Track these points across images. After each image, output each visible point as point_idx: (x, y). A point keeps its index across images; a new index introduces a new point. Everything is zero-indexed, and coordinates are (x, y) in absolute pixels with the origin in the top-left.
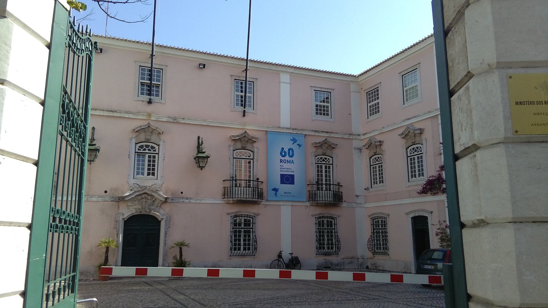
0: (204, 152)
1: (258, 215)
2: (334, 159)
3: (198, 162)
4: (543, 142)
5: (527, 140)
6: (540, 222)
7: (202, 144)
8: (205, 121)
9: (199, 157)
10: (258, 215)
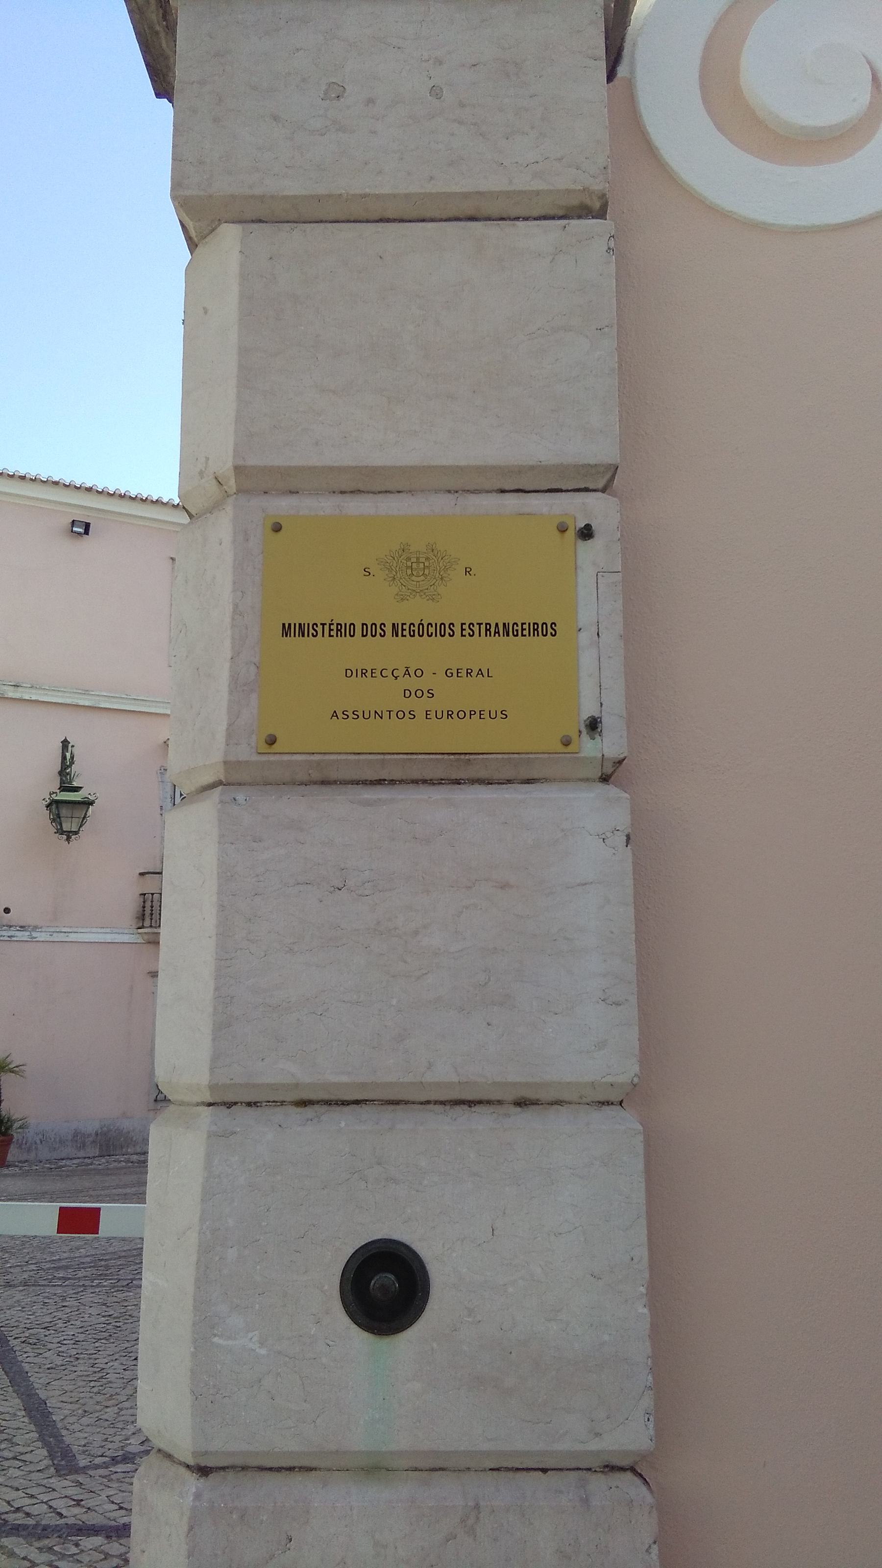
0: (77, 789)
3: (57, 819)
4: (380, 782)
5: (316, 775)
6: (328, 1103)
7: (72, 763)
8: (86, 692)
9: (57, 802)
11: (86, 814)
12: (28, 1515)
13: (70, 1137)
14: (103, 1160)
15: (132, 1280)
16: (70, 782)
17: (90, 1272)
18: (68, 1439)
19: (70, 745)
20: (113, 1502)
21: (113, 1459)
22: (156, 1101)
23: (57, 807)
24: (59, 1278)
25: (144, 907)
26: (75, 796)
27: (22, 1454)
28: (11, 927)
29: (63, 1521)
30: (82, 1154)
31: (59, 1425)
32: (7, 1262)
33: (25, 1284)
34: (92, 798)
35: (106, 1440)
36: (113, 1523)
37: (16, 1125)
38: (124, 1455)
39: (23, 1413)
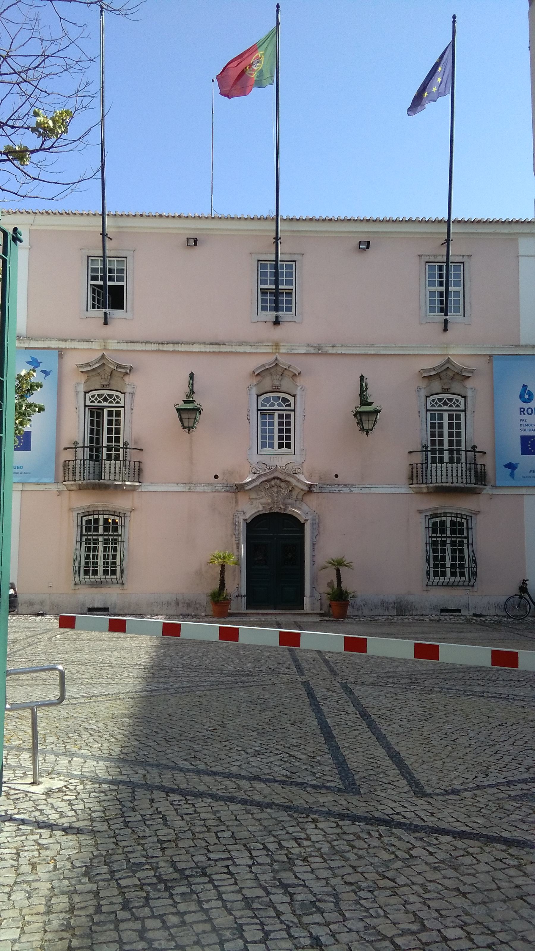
0: (371, 404)
1: (477, 513)
2: (469, 399)
3: (360, 422)
7: (367, 388)
8: (372, 346)
10: (477, 513)
11: (376, 418)
12: (405, 817)
13: (380, 604)
14: (399, 618)
15: (433, 687)
16: (366, 400)
17: (407, 680)
18: (417, 776)
19: (365, 379)
20: (452, 817)
21: (446, 791)
22: (427, 585)
23: (360, 416)
24: (391, 683)
25: (412, 472)
26: (370, 408)
27: (393, 781)
28: (339, 485)
29: (425, 824)
30: (386, 613)
31: (410, 767)
32: (360, 671)
33: (372, 684)
34: (379, 409)
35: (439, 779)
36: (456, 829)
37: (350, 596)
38: (452, 790)
39: (388, 758)
